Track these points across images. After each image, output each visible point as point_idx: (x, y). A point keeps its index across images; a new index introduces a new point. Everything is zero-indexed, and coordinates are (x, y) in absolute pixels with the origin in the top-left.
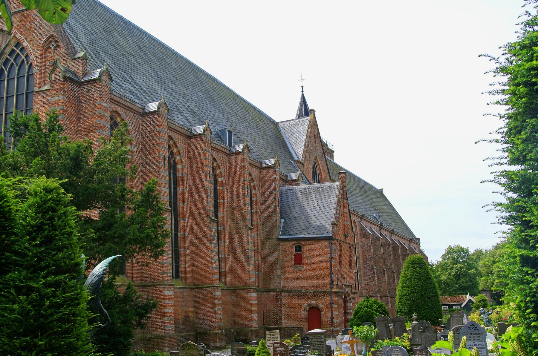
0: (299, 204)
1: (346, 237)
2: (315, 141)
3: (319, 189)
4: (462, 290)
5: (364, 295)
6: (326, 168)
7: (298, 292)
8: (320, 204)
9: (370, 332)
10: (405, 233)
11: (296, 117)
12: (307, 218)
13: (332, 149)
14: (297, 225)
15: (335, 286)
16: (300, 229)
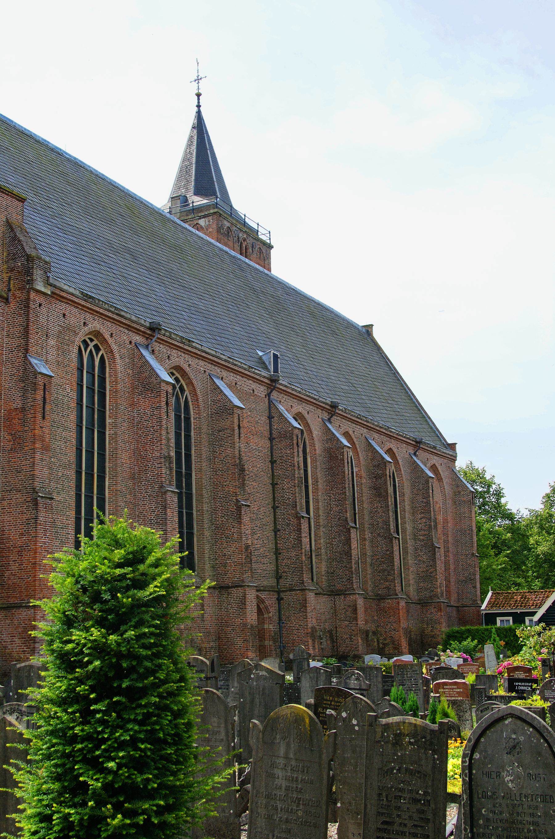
13: (268, 241)
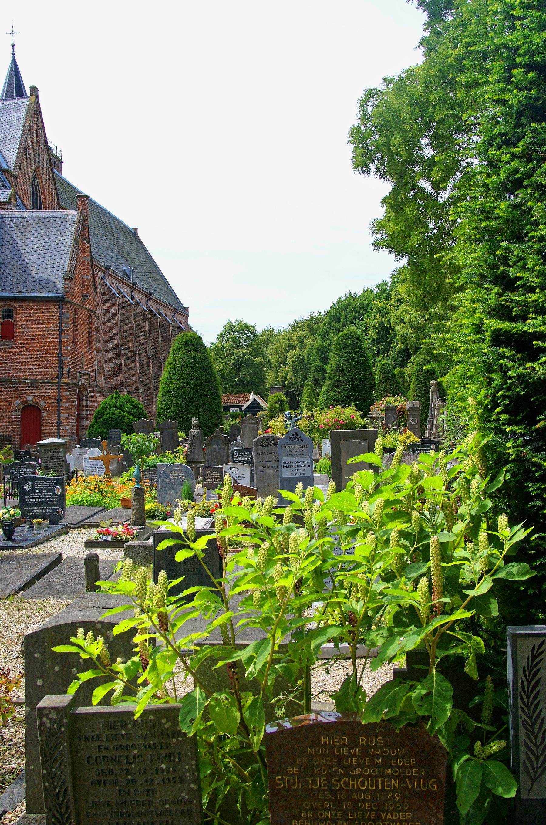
0: (11, 243)
1: (84, 299)
2: (37, 141)
3: (44, 221)
4: (242, 386)
5: (104, 389)
6: (52, 186)
7: (5, 382)
8: (45, 245)
9: (147, 443)
10: (168, 298)
11: (2, 97)
12: (23, 266)
14: (7, 275)
15: (65, 375)
16: (11, 283)
